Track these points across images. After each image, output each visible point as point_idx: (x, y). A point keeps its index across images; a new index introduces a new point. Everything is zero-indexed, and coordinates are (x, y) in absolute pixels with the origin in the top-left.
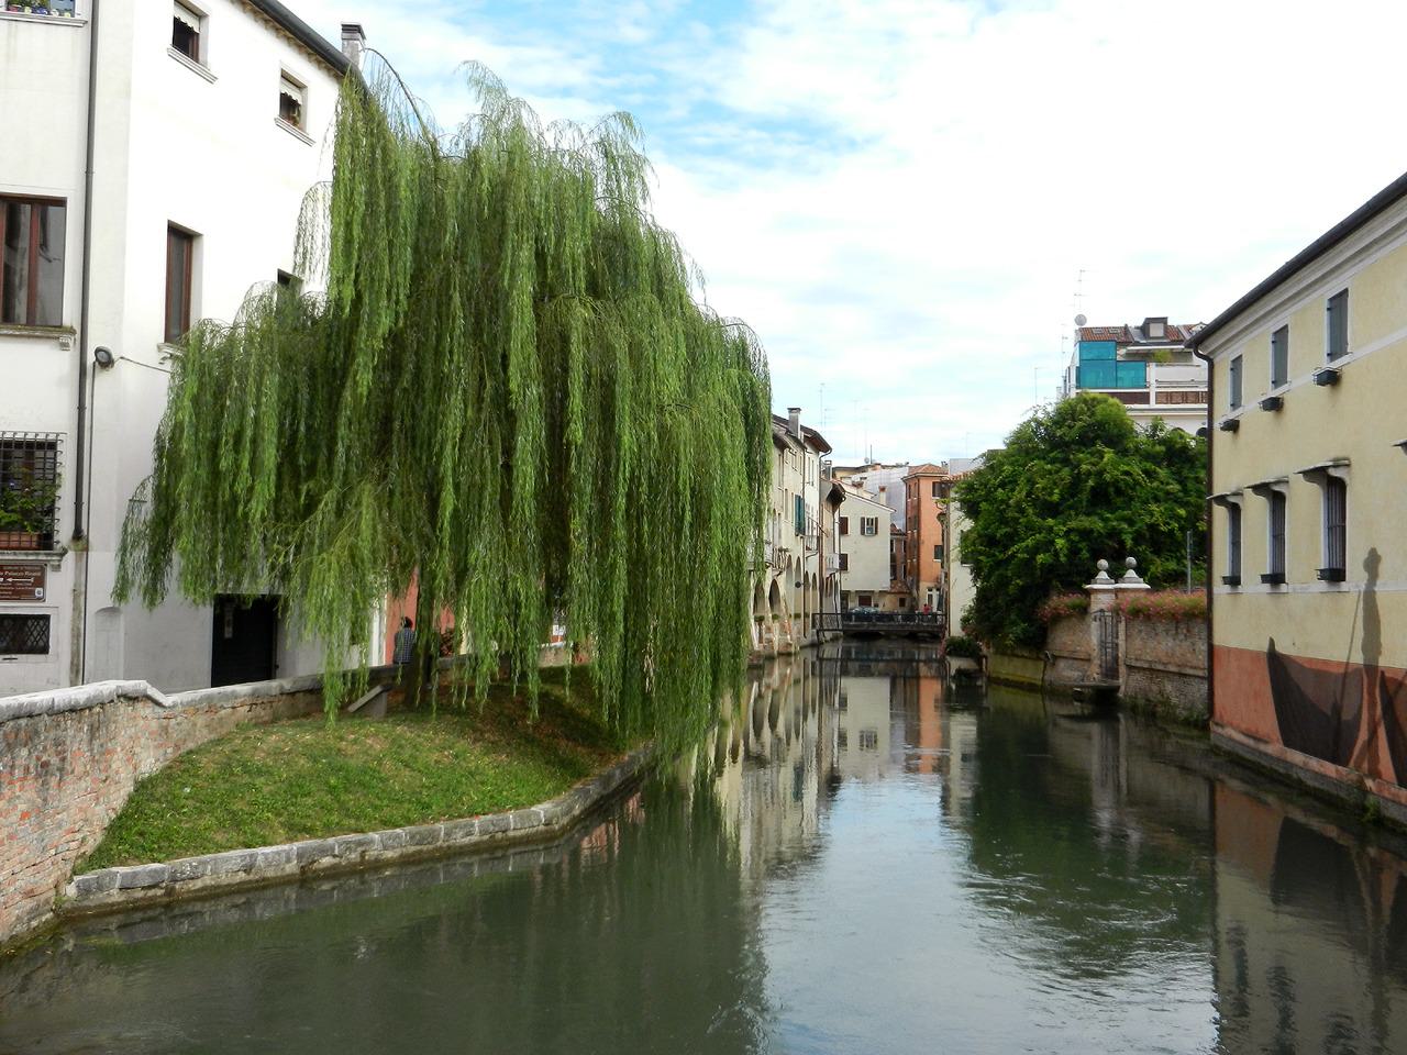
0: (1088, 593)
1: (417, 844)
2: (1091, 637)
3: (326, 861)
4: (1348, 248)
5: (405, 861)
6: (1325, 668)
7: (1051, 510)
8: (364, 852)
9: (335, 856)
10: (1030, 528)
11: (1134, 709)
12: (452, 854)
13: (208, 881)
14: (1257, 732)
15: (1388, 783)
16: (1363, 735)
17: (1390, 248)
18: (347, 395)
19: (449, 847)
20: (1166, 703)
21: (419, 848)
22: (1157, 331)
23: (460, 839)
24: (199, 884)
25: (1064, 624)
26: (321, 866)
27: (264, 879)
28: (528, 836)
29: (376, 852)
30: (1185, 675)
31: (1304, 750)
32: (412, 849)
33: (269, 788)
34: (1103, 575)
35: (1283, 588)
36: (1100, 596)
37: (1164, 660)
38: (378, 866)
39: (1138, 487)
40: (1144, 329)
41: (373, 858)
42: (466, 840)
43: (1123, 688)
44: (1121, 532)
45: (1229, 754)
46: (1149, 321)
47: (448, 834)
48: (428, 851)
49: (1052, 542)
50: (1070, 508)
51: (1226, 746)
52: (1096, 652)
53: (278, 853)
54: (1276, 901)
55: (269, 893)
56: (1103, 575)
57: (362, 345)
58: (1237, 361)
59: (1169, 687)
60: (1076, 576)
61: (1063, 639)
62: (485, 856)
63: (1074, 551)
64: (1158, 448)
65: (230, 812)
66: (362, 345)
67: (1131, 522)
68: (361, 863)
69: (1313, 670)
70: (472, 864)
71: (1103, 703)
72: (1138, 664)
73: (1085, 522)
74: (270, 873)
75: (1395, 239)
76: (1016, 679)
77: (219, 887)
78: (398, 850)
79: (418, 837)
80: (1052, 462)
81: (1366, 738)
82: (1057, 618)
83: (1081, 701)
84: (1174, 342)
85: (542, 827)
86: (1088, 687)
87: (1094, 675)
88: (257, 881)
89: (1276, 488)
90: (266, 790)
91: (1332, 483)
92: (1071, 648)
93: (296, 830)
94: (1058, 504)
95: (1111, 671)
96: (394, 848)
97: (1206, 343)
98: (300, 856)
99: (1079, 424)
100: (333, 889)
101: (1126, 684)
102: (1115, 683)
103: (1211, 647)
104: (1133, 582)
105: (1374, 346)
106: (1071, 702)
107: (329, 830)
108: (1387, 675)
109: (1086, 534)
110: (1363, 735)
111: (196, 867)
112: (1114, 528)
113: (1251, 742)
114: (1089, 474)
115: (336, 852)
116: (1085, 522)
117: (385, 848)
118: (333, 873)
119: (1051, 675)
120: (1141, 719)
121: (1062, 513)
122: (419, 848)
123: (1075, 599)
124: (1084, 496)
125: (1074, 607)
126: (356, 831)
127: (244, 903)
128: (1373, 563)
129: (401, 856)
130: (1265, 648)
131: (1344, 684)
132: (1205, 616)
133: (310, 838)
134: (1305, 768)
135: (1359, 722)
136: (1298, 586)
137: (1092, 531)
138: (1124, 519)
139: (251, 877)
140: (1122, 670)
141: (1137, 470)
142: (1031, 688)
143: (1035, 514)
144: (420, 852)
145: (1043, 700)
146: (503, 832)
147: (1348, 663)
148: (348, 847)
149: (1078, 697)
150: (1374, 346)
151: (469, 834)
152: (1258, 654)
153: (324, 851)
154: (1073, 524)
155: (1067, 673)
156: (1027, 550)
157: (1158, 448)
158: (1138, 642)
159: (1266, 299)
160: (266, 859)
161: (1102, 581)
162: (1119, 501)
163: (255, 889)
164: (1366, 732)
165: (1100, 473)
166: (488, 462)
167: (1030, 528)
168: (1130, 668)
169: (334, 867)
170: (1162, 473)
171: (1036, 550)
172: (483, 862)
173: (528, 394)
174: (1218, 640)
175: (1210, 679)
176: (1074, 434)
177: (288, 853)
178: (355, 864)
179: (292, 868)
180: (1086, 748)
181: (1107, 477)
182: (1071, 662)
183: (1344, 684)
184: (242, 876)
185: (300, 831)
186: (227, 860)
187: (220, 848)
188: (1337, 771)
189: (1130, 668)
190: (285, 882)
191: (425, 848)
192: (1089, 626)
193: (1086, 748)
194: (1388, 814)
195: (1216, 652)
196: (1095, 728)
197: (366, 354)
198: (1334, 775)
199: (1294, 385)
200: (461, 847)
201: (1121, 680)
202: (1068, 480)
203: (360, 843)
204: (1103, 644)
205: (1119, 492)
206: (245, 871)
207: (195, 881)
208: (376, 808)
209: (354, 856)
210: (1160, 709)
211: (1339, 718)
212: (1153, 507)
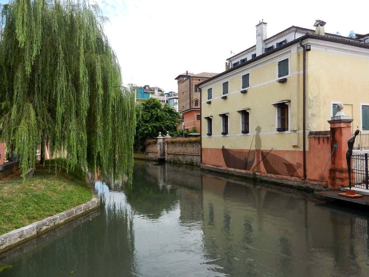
0: (157, 139)
1: (69, 217)
2: (158, 148)
3: (45, 228)
4: (251, 65)
5: (66, 223)
6: (241, 151)
7: (146, 122)
8: (55, 222)
9: (47, 226)
10: (143, 126)
11: (170, 162)
12: (78, 217)
13: (7, 244)
14: (217, 165)
15: (264, 173)
16: (255, 163)
17: (265, 64)
18: (19, 74)
19: (76, 216)
20: (180, 161)
21: (69, 218)
22: (147, 88)
23: (79, 213)
24: (4, 246)
25: (151, 145)
26: (43, 230)
27: (26, 239)
28: (94, 208)
29: (58, 222)
30: (185, 155)
31: (234, 168)
32: (67, 218)
33: (15, 205)
34: (160, 135)
35: (227, 135)
36: (160, 139)
37: (179, 152)
38: (58, 226)
39: (164, 117)
40: (145, 87)
41: (57, 224)
42: (80, 213)
43: (166, 158)
44: (162, 126)
45: (208, 170)
46: (146, 86)
47: (76, 212)
48: (72, 218)
49: (148, 128)
50: (151, 121)
51: (207, 168)
52: (159, 152)
53: (30, 228)
54: (224, 198)
55: (28, 243)
56: (160, 135)
57: (27, 58)
58: (210, 91)
59: (180, 157)
60: (153, 135)
61: (150, 149)
62: (85, 216)
63: (153, 131)
64: (167, 109)
65: (6, 217)
66: (27, 58)
67: (164, 124)
68: (54, 226)
69: (238, 151)
70: (81, 220)
71: (161, 162)
72: (171, 153)
73: (154, 124)
74: (28, 236)
75: (346, 52)
76: (137, 158)
77: (11, 245)
78: (64, 219)
79: (69, 214)
80: (146, 112)
81: (256, 164)
82: (150, 144)
83: (155, 161)
84: (150, 90)
85: (97, 205)
86: (157, 158)
87: (159, 156)
88: (24, 240)
89: (227, 115)
90: (15, 206)
91: (245, 114)
92: (152, 151)
93: (32, 219)
94: (148, 120)
95: (163, 154)
96: (63, 219)
97: (200, 86)
98: (37, 228)
99: (151, 104)
100: (47, 236)
101: (167, 157)
102: (164, 157)
103: (201, 148)
104: (168, 136)
105: (254, 86)
106: (153, 162)
107: (42, 217)
108: (263, 151)
109: (155, 127)
110: (255, 163)
111: (3, 240)
112: (160, 126)
113: (216, 167)
114: (155, 114)
115: (47, 224)
116: (154, 124)
117: (61, 219)
118: (47, 232)
119: (147, 156)
120: (172, 164)
121: (149, 122)
122: (69, 218)
123: (155, 140)
124: (154, 119)
125: (154, 142)
126: (50, 216)
127: (20, 249)
128: (258, 129)
129: (65, 221)
130: (221, 148)
131: (249, 154)
132: (200, 142)
133: (37, 221)
134: (234, 171)
135: (254, 161)
136: (233, 135)
137: (156, 126)
138: (161, 124)
139: (22, 239)
140: (166, 154)
141: (164, 113)
142: (142, 159)
143: (144, 123)
144: (69, 219)
145: (145, 162)
146: (88, 208)
147: (250, 150)
148: (51, 221)
149: (155, 161)
150: (254, 86)
151: (81, 210)
152: (218, 149)
153: (44, 224)
154: (152, 125)
155: (150, 155)
156: (142, 130)
157: (167, 109)
158: (171, 149)
159: (227, 74)
160: (27, 231)
161: (160, 136)
162: (160, 120)
163: (24, 243)
164: (256, 163)
165: (157, 114)
166: (72, 98)
167: (143, 126)
168: (168, 154)
169: (47, 229)
170: (168, 114)
171: (144, 130)
172: (84, 218)
173: (84, 78)
174: (203, 147)
175: (201, 156)
176: (150, 106)
177: (33, 228)
178: (52, 227)
179: (34, 233)
180: (157, 171)
181: (159, 115)
182: (152, 153)
183: (249, 154)
184: (19, 239)
185: (32, 219)
186: (13, 235)
187: (7, 231)
188: (246, 171)
189: (168, 154)
190: (33, 238)
191: (70, 217)
192: (157, 146)
193: (157, 171)
194: (263, 179)
195: (202, 149)
196: (159, 167)
197: (28, 61)
198: (245, 172)
199: (230, 94)
200: (79, 215)
201: (166, 157)
202: (150, 115)
203: (54, 220)
204: (161, 149)
205: (161, 118)
206: (20, 237)
207: (3, 245)
208: (52, 207)
209: (52, 224)
210: (178, 162)
211: (247, 161)
212: (168, 121)
